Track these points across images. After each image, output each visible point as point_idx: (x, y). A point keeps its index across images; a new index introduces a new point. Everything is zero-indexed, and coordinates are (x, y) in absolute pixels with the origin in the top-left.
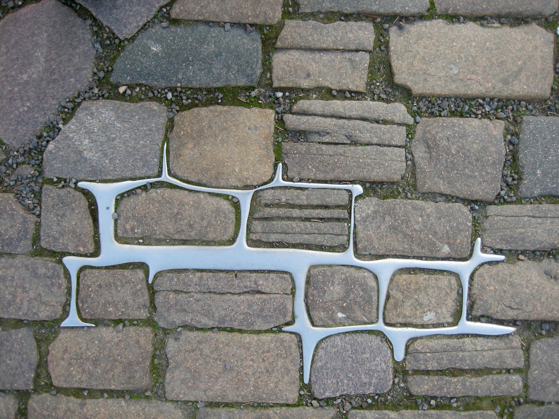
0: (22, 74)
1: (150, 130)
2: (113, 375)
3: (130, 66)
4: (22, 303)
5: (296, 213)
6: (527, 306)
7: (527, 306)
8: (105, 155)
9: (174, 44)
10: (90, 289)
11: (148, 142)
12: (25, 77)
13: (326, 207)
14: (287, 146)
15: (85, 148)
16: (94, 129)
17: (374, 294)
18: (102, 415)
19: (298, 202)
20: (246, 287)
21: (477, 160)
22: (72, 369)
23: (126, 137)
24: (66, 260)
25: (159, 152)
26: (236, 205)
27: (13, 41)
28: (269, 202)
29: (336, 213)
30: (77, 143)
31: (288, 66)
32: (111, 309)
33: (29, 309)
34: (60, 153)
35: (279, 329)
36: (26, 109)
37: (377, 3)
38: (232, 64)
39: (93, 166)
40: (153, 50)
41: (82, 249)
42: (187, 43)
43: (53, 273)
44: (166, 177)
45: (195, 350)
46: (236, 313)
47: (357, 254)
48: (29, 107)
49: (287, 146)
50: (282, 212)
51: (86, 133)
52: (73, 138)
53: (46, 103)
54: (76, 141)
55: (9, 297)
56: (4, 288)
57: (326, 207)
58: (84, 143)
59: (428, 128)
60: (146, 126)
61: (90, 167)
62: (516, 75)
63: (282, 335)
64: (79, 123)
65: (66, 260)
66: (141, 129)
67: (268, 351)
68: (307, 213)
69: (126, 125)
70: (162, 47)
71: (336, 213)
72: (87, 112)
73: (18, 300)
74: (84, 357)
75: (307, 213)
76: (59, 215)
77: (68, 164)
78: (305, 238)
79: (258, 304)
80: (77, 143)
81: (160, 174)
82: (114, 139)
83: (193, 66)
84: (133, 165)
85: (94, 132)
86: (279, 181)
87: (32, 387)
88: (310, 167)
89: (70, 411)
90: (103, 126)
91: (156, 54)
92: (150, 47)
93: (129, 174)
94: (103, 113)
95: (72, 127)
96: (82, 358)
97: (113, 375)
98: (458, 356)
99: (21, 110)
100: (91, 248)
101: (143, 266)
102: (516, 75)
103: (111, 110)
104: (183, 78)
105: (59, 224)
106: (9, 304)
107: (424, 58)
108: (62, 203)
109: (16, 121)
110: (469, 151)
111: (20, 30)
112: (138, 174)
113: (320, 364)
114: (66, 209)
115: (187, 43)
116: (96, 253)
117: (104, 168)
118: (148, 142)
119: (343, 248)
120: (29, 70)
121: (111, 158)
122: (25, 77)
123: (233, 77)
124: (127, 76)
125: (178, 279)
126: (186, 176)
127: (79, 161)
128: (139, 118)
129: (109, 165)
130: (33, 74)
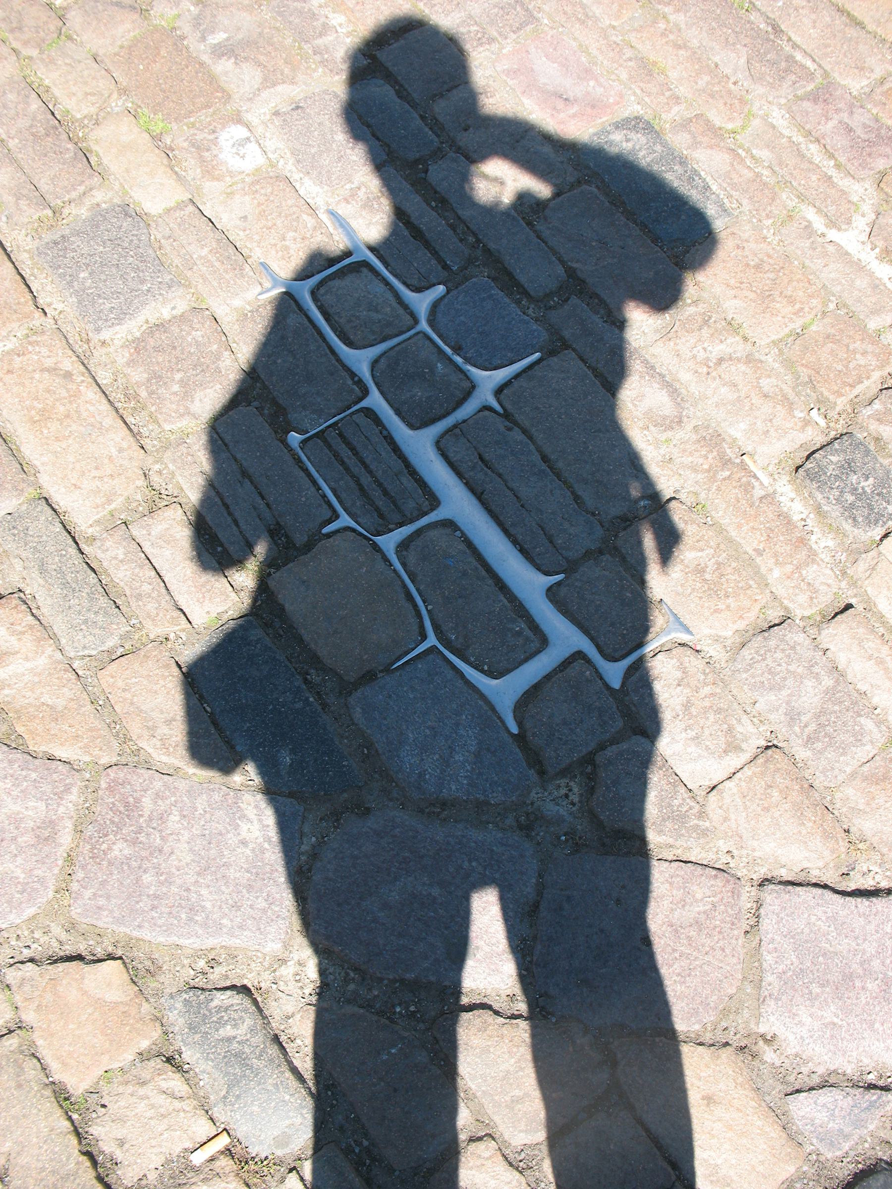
0: (435, 898)
1: (390, 697)
2: (698, 541)
3: (328, 772)
4: (706, 697)
5: (366, 480)
6: (294, 213)
7: (294, 213)
8: (457, 724)
9: (265, 740)
10: (625, 632)
11: (405, 689)
12: (436, 892)
13: (336, 455)
14: (300, 539)
15: (467, 754)
16: (437, 760)
17: (393, 353)
18: (752, 524)
19: (352, 484)
20: (486, 474)
21: (174, 348)
22: (730, 590)
23: (418, 717)
24: (616, 684)
25: (408, 668)
26: (403, 547)
27: (401, 942)
28: (375, 515)
29: (337, 444)
30: (469, 768)
31: (204, 597)
32: (628, 594)
33: (706, 684)
34: (496, 779)
35: (507, 415)
36: (474, 864)
37: (64, 553)
38: (244, 658)
39: (481, 730)
40: (291, 759)
41: (588, 673)
42: (254, 726)
43: (642, 687)
44: (432, 640)
45: (597, 481)
46: (523, 465)
47: (366, 392)
48: (470, 861)
49: (300, 539)
50: (376, 494)
51: (448, 766)
52: (466, 777)
53: (448, 843)
54: (467, 771)
55: (712, 717)
56: (706, 730)
57: (336, 455)
58: (461, 759)
59: (173, 414)
60: (388, 704)
61: (486, 732)
62: (53, 370)
63: (509, 407)
64: (443, 783)
65: (616, 684)
66: (396, 709)
67: (537, 408)
68: (358, 470)
69: (404, 727)
70: (278, 751)
71: (337, 444)
72: (422, 784)
73: (707, 703)
74: (706, 586)
75: (358, 470)
76: (570, 729)
77: (501, 760)
78: (385, 451)
79: (495, 451)
80: (469, 768)
81: (433, 649)
82: (432, 728)
83: (277, 699)
84: (445, 687)
85: (441, 757)
86: (345, 520)
87: (757, 561)
88: (303, 499)
89: (777, 560)
90: (426, 752)
91: (293, 751)
92: (290, 765)
93: (459, 683)
94: (410, 764)
95: (454, 788)
96: (709, 589)
97: (698, 541)
98: (395, 239)
99: (480, 869)
100: (578, 664)
101: (552, 593)
102: (53, 370)
103: (399, 757)
104: (300, 700)
105: (582, 721)
106: (719, 711)
107: (97, 468)
108: (554, 735)
109: (499, 867)
110: (169, 361)
111: (381, 942)
112: (450, 674)
113: (509, 354)
114: (557, 725)
115: (254, 726)
116: (579, 655)
117: (473, 715)
118: (405, 689)
119: (369, 413)
120: (424, 893)
121: (456, 715)
122: (436, 892)
123: (259, 646)
124: (344, 766)
125: (535, 548)
126: (413, 620)
127: (488, 750)
128: (385, 719)
129: (466, 712)
130: (424, 884)
